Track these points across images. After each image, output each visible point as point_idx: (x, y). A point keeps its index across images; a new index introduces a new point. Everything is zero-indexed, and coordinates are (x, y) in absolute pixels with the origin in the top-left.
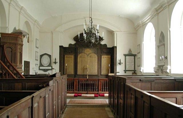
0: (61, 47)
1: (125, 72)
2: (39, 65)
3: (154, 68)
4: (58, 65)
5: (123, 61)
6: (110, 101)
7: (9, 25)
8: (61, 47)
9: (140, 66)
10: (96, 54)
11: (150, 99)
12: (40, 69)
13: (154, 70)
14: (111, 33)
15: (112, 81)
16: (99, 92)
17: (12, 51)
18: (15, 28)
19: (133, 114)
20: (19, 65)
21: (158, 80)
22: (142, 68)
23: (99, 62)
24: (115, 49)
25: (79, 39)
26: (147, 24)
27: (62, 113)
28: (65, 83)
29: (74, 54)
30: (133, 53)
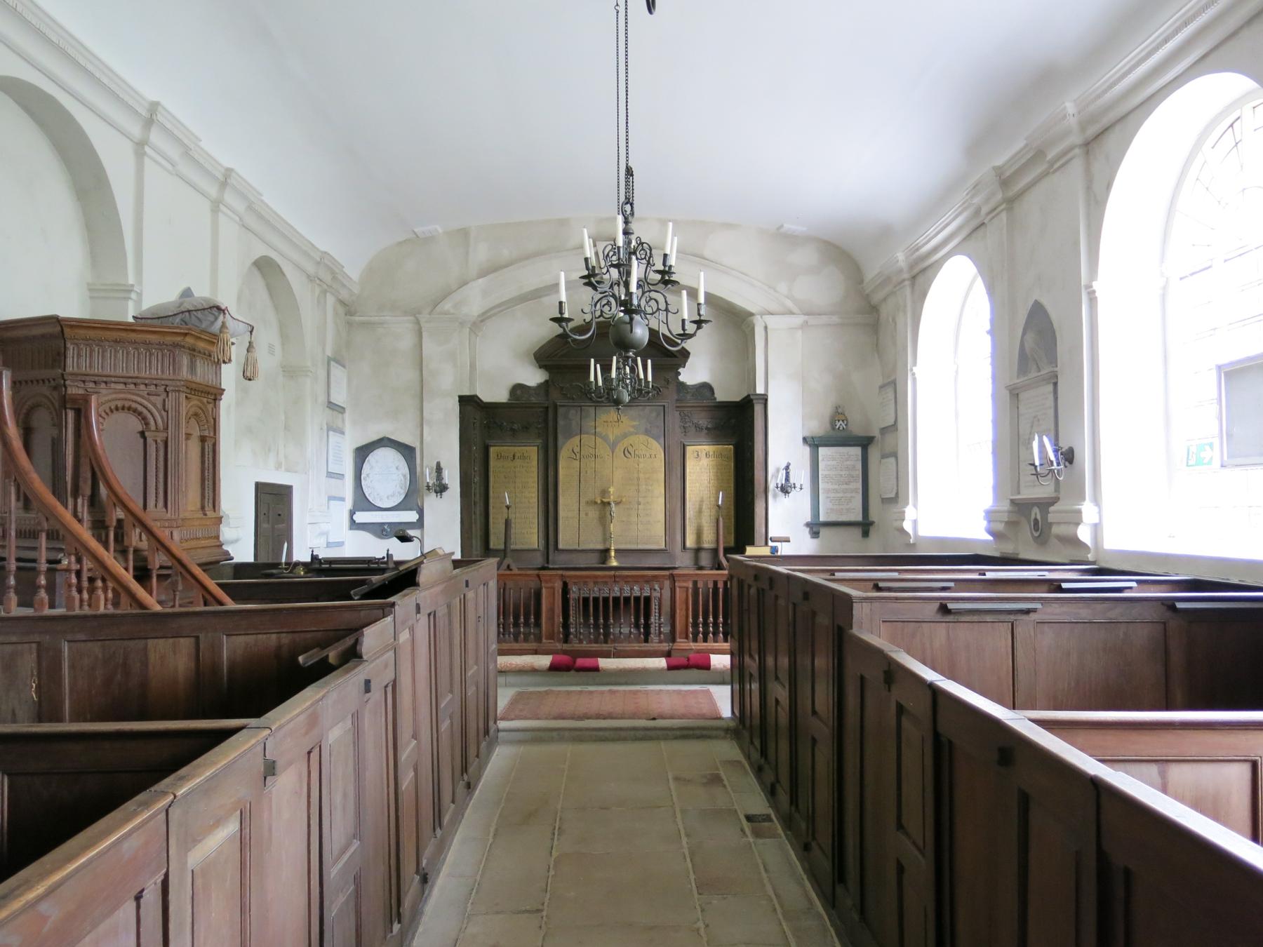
0: (468, 402)
1: (815, 534)
2: (349, 504)
3: (990, 515)
4: (453, 497)
5: (801, 476)
6: (740, 699)
7: (140, 281)
8: (468, 402)
9: (896, 499)
10: (656, 438)
11: (1098, 796)
12: (354, 525)
13: (985, 523)
14: (736, 324)
15: (753, 591)
16: (676, 646)
17: (142, 434)
18: (187, 293)
19: (924, 855)
20: (200, 515)
21: (1056, 608)
22: (910, 512)
23: (677, 484)
24: (758, 409)
25: (565, 355)
26: (938, 264)
27: (468, 786)
28: (486, 609)
29: (539, 441)
30: (857, 429)
